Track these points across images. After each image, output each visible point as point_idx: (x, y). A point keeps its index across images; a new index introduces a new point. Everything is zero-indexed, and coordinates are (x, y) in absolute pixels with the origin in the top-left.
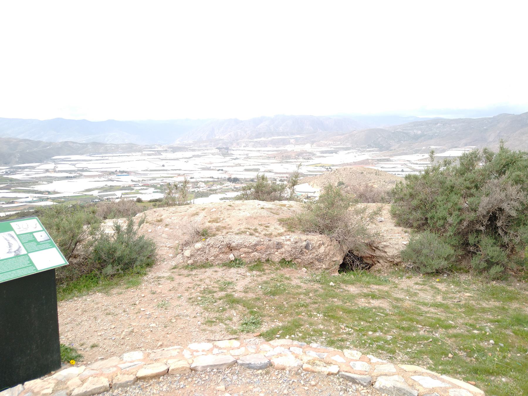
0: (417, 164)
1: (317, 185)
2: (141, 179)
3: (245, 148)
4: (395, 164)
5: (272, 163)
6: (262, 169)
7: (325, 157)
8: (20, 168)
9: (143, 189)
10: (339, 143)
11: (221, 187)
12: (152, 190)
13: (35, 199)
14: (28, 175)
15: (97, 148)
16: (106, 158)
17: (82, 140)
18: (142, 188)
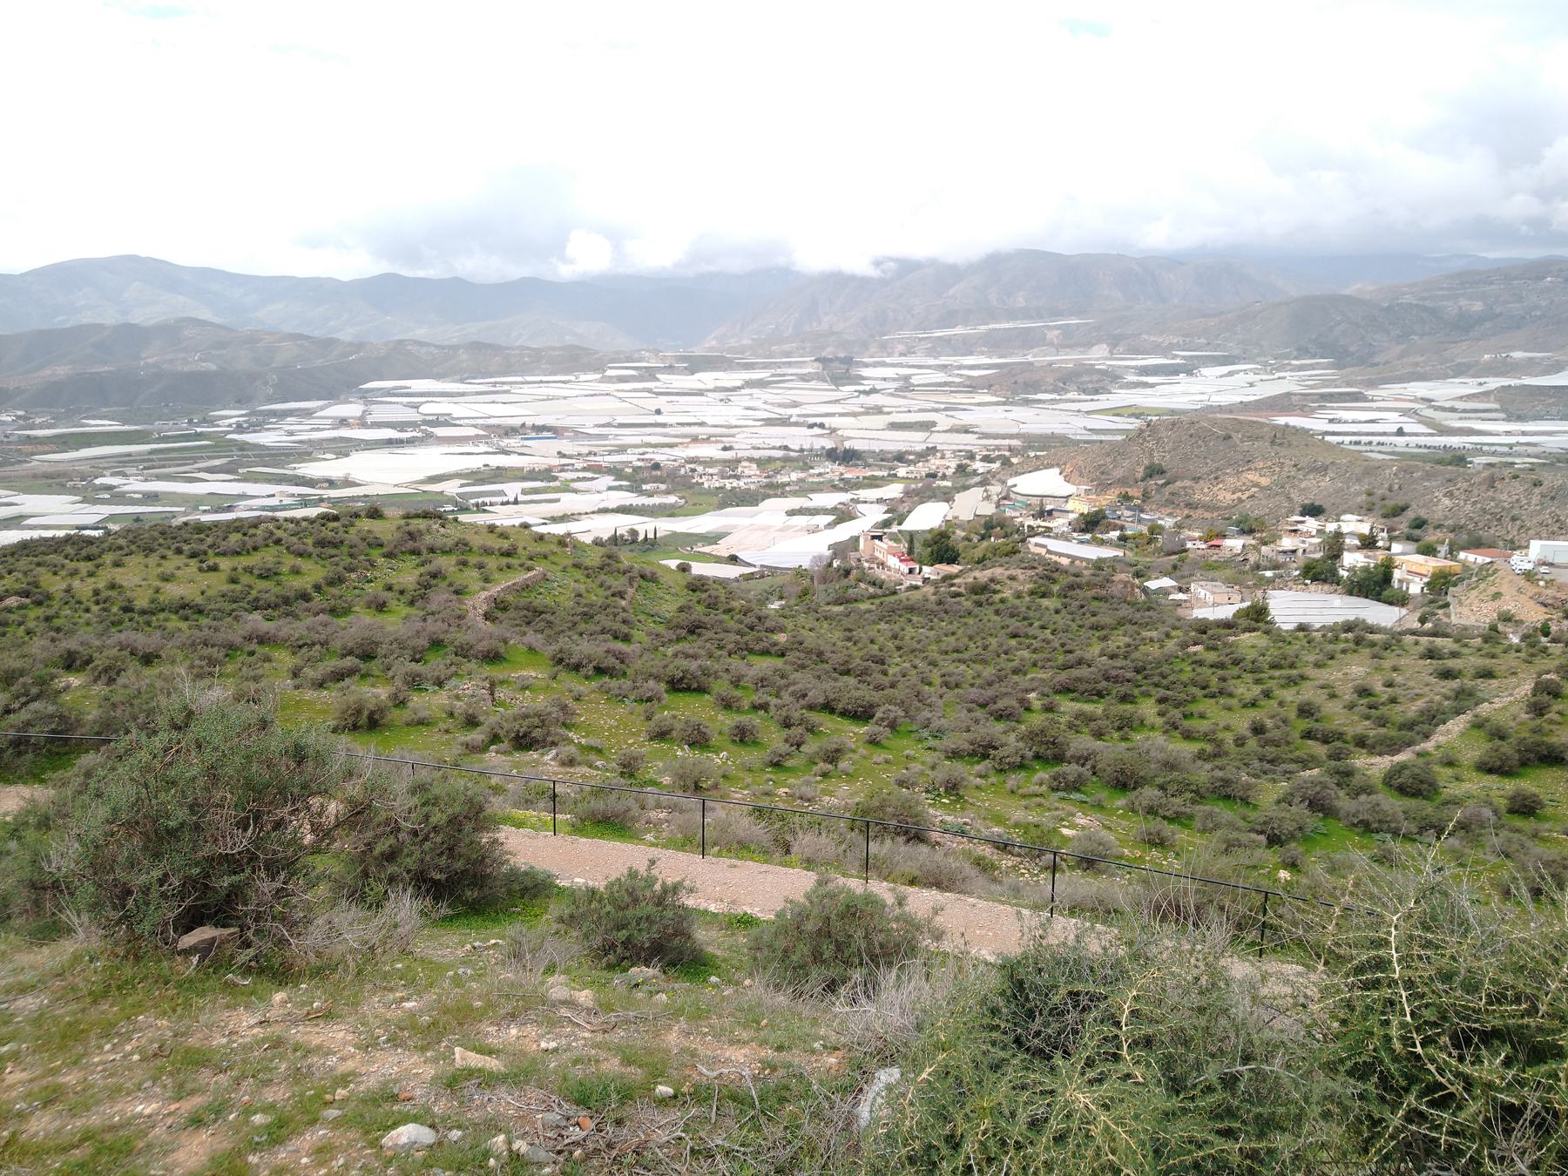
0: (1453, 410)
1: (1081, 475)
2: (585, 450)
3: (903, 360)
4: (1379, 409)
5: (979, 404)
6: (943, 421)
7: (1152, 386)
8: (274, 413)
9: (584, 479)
10: (1203, 341)
11: (802, 475)
12: (609, 480)
13: (287, 501)
14: (291, 433)
15: (487, 361)
16: (506, 387)
17: (450, 333)
18: (581, 475)
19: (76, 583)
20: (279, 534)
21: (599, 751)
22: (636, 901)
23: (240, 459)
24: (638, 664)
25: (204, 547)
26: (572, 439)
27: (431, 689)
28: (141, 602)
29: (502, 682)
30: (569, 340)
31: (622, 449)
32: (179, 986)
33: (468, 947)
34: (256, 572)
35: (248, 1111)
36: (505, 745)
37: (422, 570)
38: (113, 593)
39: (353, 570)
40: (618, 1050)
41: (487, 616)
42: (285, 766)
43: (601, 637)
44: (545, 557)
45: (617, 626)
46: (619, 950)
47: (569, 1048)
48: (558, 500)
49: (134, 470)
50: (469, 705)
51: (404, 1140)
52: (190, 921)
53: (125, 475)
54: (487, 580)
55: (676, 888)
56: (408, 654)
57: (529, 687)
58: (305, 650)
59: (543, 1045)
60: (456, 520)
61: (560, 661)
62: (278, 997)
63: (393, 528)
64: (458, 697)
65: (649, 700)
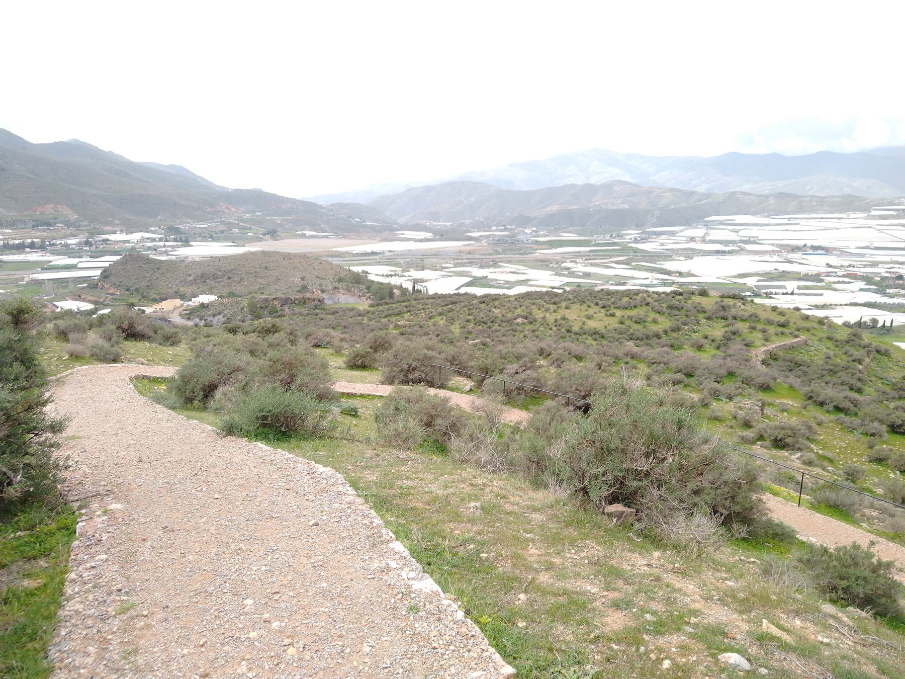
2: (846, 263)
8: (655, 233)
9: (843, 282)
12: (861, 284)
13: (655, 282)
14: (662, 245)
16: (797, 221)
17: (765, 187)
18: (841, 279)
19: (548, 315)
20: (649, 300)
21: (831, 461)
22: (857, 565)
23: (633, 257)
24: (867, 410)
25: (609, 303)
26: (838, 256)
27: (724, 400)
28: (576, 329)
29: (770, 404)
30: (847, 191)
31: (875, 264)
32: (606, 531)
33: (737, 558)
34: (634, 319)
35: (643, 610)
36: (767, 443)
37: (727, 329)
38: (563, 322)
39: (686, 324)
40: (874, 661)
41: (764, 362)
42: (671, 429)
43: (841, 387)
44: (808, 330)
45: (853, 381)
46: (840, 592)
47: (837, 647)
48: (821, 295)
49: (580, 260)
50: (747, 414)
51: (732, 661)
52: (613, 499)
53: (576, 262)
54: (767, 340)
55: (889, 565)
56: (713, 377)
57: (787, 410)
58: (655, 365)
59: (820, 638)
60: (752, 301)
61: (811, 398)
62: (657, 554)
63: (713, 303)
64: (740, 408)
65: (873, 435)
